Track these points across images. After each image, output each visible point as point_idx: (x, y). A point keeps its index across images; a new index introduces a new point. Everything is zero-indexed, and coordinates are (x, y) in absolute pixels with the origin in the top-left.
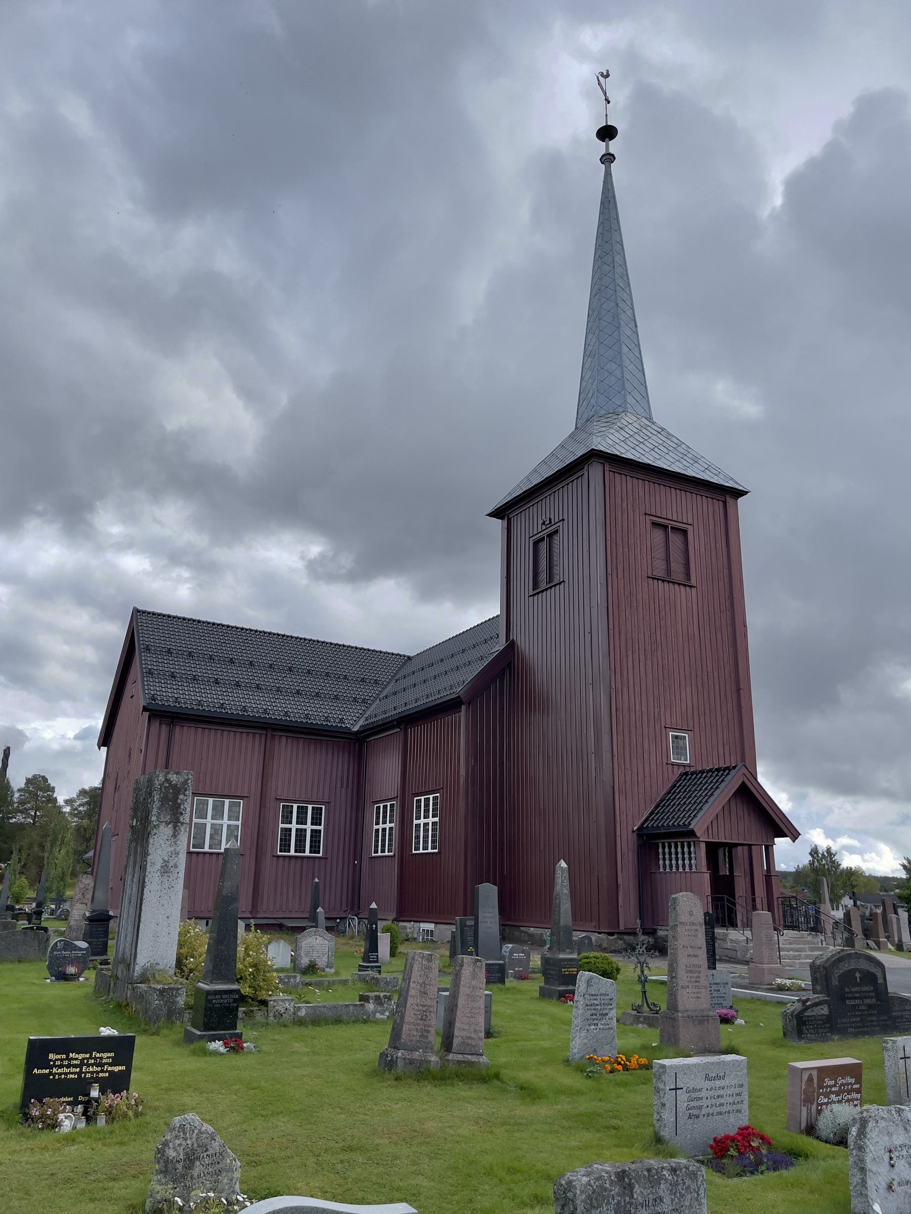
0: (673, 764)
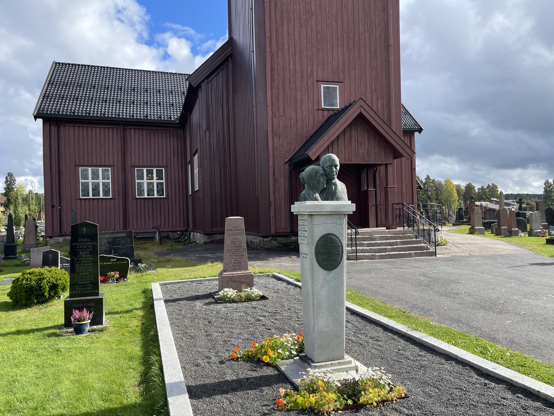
0: (323, 110)
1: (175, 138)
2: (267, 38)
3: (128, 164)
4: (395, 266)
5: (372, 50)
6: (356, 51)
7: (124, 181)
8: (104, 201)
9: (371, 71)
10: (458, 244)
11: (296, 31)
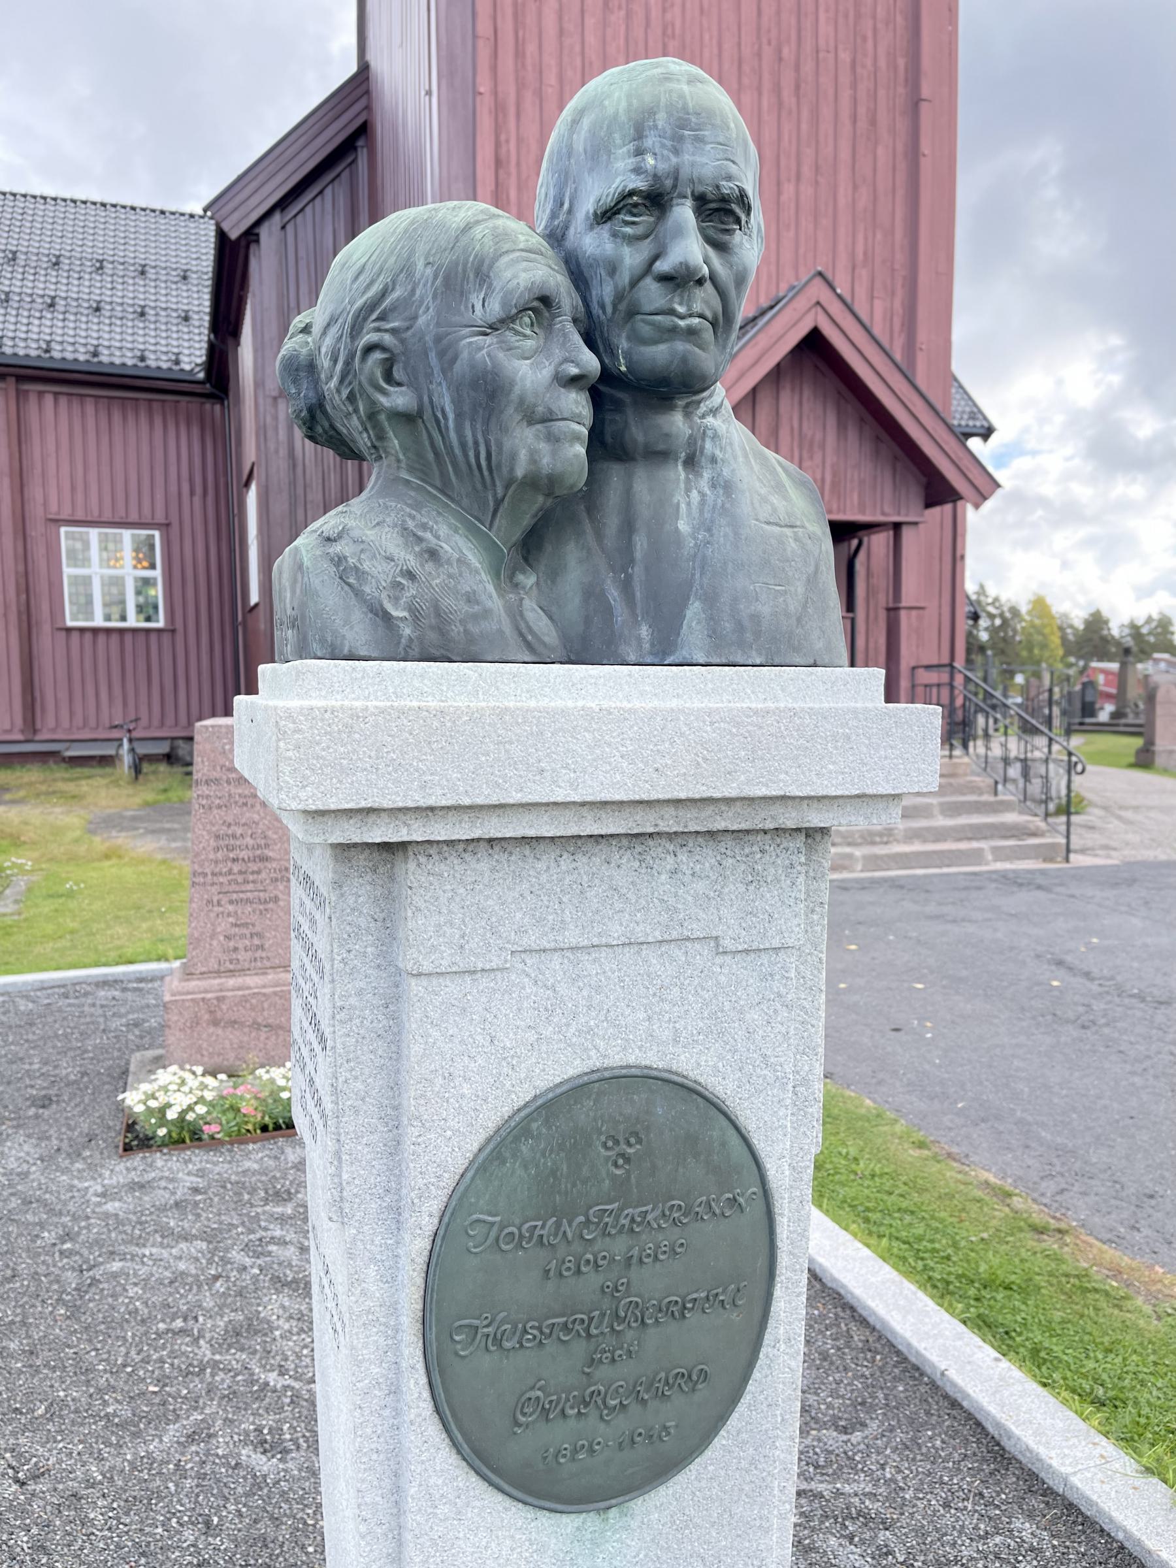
1: (196, 431)
2: (481, 43)
3: (36, 511)
4: (931, 909)
5: (862, 111)
6: (805, 114)
7: (21, 568)
8: (141, 638)
9: (855, 187)
10: (1121, 808)
11: (590, 22)
